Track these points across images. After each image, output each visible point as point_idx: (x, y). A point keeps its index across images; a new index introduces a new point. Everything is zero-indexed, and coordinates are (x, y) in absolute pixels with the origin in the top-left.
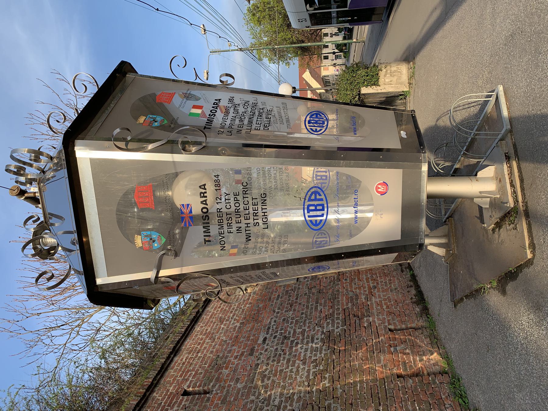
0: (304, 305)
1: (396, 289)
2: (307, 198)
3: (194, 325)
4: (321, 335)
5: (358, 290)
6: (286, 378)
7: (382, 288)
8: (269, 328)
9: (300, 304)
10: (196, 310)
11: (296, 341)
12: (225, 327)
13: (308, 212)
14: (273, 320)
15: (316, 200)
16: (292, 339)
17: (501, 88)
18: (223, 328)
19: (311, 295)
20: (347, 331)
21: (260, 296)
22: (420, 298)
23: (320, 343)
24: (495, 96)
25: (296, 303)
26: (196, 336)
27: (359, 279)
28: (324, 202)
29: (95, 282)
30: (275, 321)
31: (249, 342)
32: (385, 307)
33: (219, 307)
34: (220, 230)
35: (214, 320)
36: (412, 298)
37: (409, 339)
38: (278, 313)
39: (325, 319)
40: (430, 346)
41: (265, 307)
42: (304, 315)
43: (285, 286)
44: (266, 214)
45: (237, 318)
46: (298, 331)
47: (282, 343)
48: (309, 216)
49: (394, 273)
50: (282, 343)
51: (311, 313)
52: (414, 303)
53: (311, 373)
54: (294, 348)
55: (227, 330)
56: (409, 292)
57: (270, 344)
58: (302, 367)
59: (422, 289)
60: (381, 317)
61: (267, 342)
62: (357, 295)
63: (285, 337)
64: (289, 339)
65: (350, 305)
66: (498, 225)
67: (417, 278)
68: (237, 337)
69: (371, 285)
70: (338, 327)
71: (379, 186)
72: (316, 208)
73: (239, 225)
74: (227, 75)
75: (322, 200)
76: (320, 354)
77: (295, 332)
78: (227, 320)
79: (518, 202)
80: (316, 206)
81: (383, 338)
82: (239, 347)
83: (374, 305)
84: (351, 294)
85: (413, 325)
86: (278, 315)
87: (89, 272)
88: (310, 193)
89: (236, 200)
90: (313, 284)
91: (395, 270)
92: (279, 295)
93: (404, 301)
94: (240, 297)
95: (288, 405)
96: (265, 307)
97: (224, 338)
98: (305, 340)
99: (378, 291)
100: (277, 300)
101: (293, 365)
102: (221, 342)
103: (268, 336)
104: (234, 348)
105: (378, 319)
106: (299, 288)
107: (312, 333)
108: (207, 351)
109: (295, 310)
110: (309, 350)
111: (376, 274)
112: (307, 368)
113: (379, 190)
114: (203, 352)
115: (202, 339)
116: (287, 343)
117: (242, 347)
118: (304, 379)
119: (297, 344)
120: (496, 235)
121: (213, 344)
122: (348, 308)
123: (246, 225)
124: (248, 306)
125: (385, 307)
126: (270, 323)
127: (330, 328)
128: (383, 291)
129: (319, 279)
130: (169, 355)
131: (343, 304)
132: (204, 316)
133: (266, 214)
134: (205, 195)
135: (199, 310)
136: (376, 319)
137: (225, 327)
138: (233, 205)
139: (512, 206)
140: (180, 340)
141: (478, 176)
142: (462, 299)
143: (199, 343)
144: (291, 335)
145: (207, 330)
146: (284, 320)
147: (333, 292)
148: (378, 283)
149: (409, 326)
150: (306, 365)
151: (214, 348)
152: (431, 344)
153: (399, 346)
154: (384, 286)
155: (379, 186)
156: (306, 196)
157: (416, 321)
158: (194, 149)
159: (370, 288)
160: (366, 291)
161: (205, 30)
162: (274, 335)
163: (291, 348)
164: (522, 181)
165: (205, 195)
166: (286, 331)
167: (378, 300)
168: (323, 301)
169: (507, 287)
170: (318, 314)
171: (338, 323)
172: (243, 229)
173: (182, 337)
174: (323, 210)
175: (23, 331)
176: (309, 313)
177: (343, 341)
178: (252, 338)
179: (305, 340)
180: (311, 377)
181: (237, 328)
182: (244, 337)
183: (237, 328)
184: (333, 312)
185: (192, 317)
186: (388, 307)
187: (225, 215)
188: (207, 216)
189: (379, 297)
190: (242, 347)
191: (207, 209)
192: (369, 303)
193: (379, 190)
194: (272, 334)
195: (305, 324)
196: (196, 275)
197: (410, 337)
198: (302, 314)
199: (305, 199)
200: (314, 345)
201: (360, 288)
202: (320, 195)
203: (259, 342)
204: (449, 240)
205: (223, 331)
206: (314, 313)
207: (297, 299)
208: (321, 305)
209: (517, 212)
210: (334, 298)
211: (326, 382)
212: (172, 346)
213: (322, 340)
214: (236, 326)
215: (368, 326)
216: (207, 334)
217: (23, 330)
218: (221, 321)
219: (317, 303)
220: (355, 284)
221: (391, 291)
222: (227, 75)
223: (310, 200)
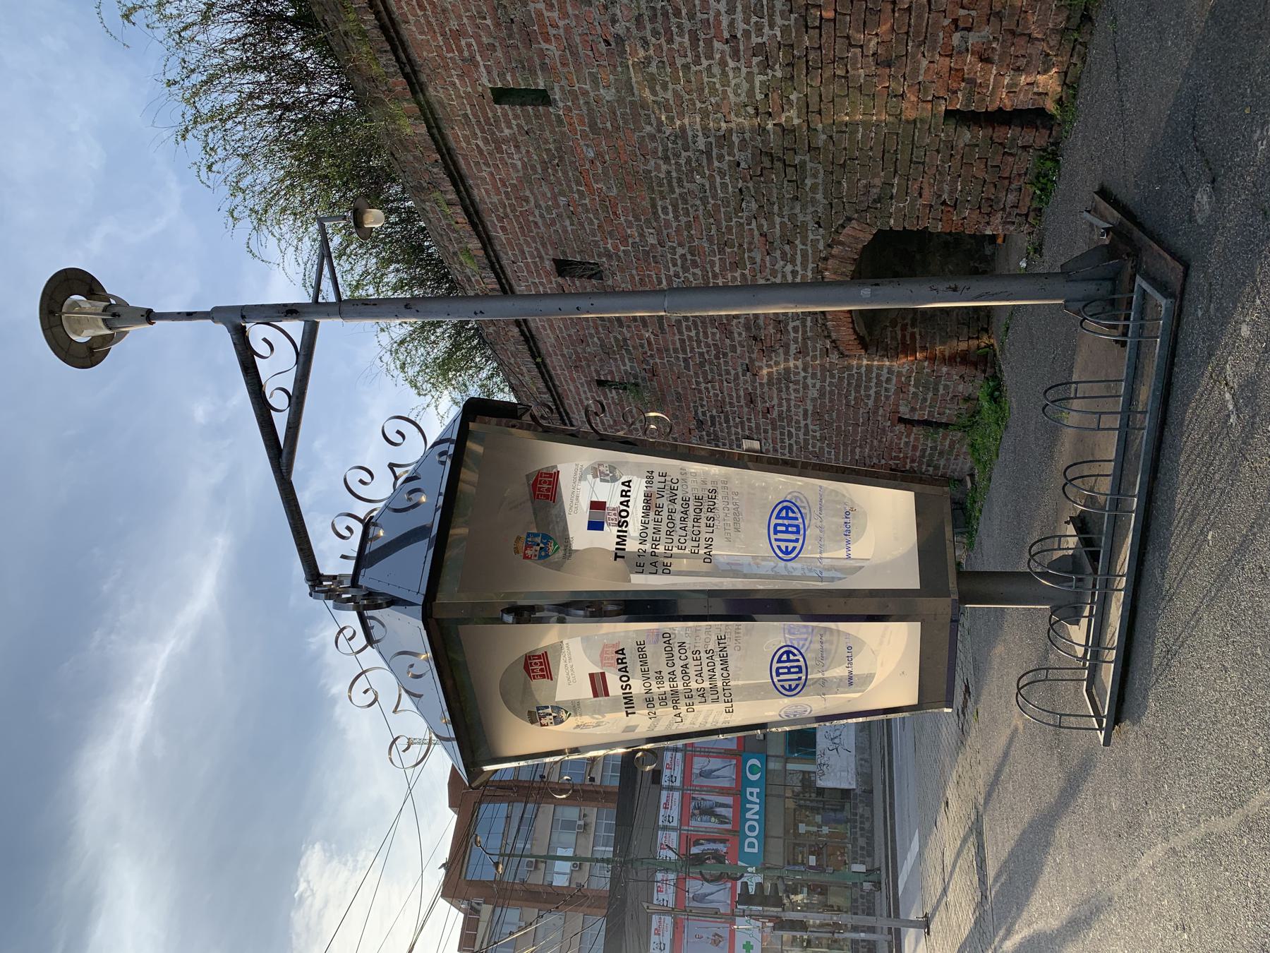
6: (703, 90)
15: (787, 518)
53: (757, 84)
58: (731, 64)
74: (343, 537)
75: (796, 519)
76: (771, 26)
80: (787, 526)
95: (725, 151)
101: (710, 57)
112: (744, 70)
118: (743, 98)
150: (742, 61)
161: (395, 740)
180: (759, 97)
211: (793, 113)
222: (343, 537)
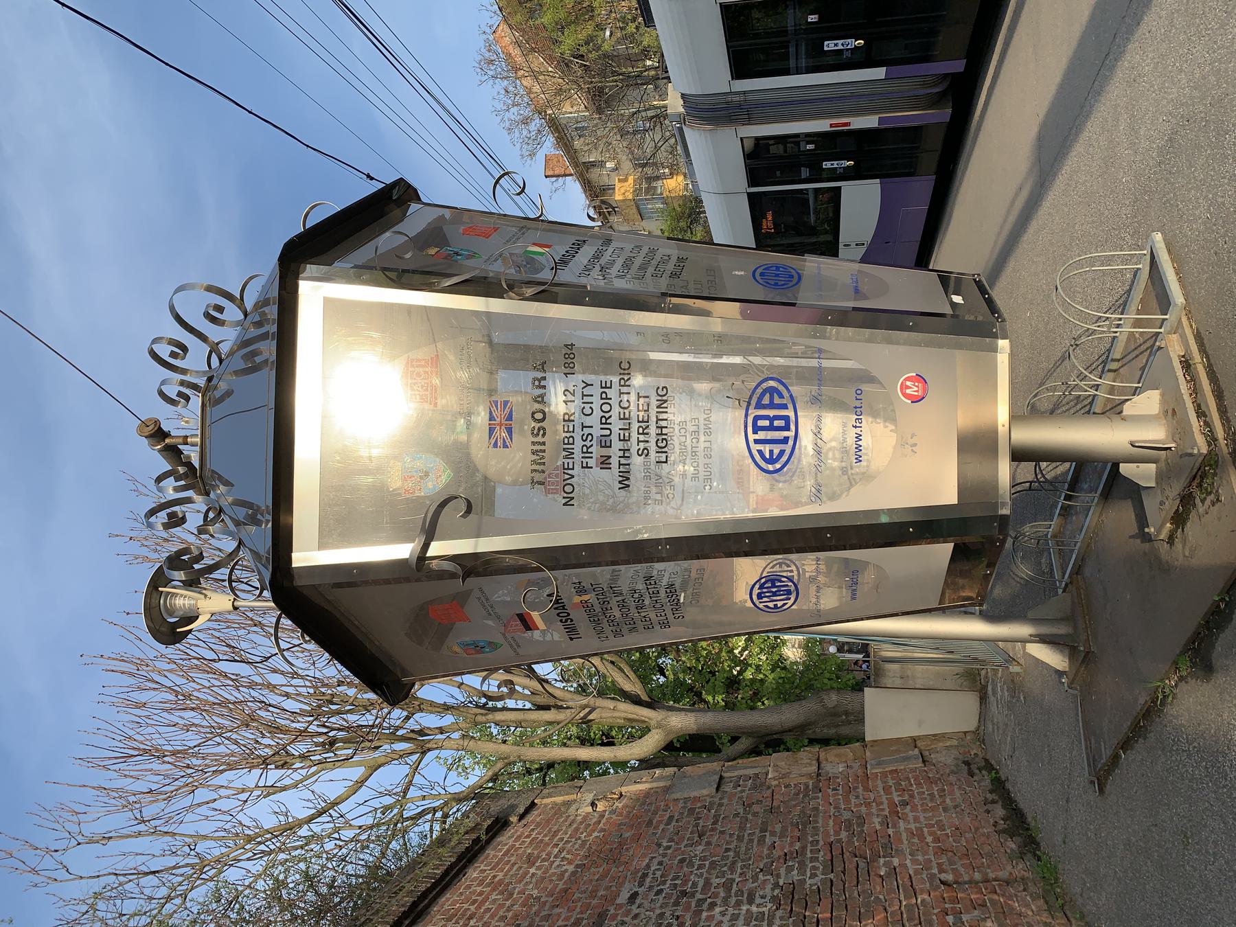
0: (731, 835)
1: (955, 807)
2: (754, 402)
3: (465, 867)
4: (773, 890)
5: (863, 809)
7: (922, 805)
8: (645, 876)
9: (722, 832)
10: (474, 836)
11: (709, 900)
12: (539, 873)
13: (755, 432)
14: (655, 861)
15: (772, 406)
16: (699, 896)
17: (1158, 237)
18: (533, 874)
19: (750, 816)
20: (838, 885)
21: (627, 817)
22: (1017, 823)
23: (769, 905)
24: (1148, 257)
25: (712, 830)
26: (469, 887)
27: (866, 789)
28: (791, 414)
29: (289, 560)
30: (660, 863)
31: (594, 902)
32: (929, 839)
33: (528, 836)
34: (566, 461)
35: (513, 859)
36: (995, 824)
37: (991, 900)
38: (669, 848)
39: (782, 861)
40: (1045, 914)
41: (637, 838)
42: (731, 854)
43: (686, 800)
44: (665, 431)
45: (569, 856)
46: (715, 881)
47: (676, 904)
48: (756, 442)
49: (952, 778)
50: (676, 904)
51: (747, 849)
52: (1004, 831)
54: (705, 914)
55: (543, 878)
56: (988, 812)
57: (646, 904)
59: (1021, 805)
60: (920, 858)
61: (638, 901)
62: (860, 817)
63: (684, 893)
64: (693, 895)
65: (844, 835)
66: (1179, 519)
67: (1008, 786)
68: (566, 891)
69: (897, 799)
70: (813, 876)
71: (908, 383)
72: (771, 423)
73: (605, 452)
75: (785, 407)
77: (707, 883)
78: (544, 860)
79: (1215, 440)
80: (772, 419)
81: (926, 896)
82: (571, 910)
83: (904, 836)
84: (847, 815)
85: (1002, 874)
86: (669, 851)
87: (282, 541)
88: (759, 391)
89: (605, 398)
90: (756, 796)
91: (953, 772)
92: (671, 818)
93: (977, 829)
94: (579, 818)
96: (637, 838)
97: (536, 891)
98: (733, 900)
99: (914, 809)
100: (668, 824)
102: (527, 899)
103: (641, 890)
104: (557, 910)
105: (914, 862)
106: (720, 805)
107: (750, 885)
108: (492, 917)
109: (709, 843)
110: (742, 918)
111: (908, 779)
113: (908, 391)
114: (482, 918)
115: (480, 894)
116: (689, 904)
117: (578, 910)
119: (712, 906)
120: (1178, 545)
121: (508, 903)
122: (839, 841)
123: (621, 453)
124: (596, 834)
125: (929, 839)
126: (648, 866)
127: (795, 876)
128: (924, 811)
129: (769, 788)
130: (400, 918)
131: (827, 834)
132: (490, 852)
133: (665, 431)
134: (543, 383)
135: (478, 838)
136: (908, 862)
137: (539, 873)
138: (596, 406)
139: (1204, 450)
140: (428, 891)
141: (1124, 413)
142: (1115, 758)
143: (474, 902)
144: (699, 889)
145: (495, 877)
146: (682, 861)
147: (802, 811)
148: (912, 796)
149: (991, 875)
151: (508, 911)
152: (1049, 910)
153: (968, 912)
154: (927, 801)
155: (908, 383)
156: (751, 398)
157: (1009, 868)
158: (529, 291)
159: (892, 804)
160: (883, 810)
162: (656, 889)
163: (698, 913)
164: (1219, 395)
165: (543, 383)
166: (685, 882)
167: (912, 826)
168: (778, 828)
169: (1214, 655)
170: (766, 852)
171: (814, 868)
172: (614, 461)
173: (434, 886)
174: (787, 428)
175: (62, 874)
176: (743, 849)
177: (826, 903)
178: (602, 893)
179: (733, 900)
181: (567, 875)
182: (582, 893)
183: (567, 875)
184: (804, 848)
185: (462, 848)
186: (937, 840)
187: (578, 429)
188: (544, 429)
189: (916, 820)
190: (578, 910)
191: (544, 413)
192: (890, 831)
193: (908, 391)
194: (651, 888)
195: (732, 868)
196: (509, 559)
197: (996, 897)
198: (727, 850)
199: (749, 404)
200: (754, 909)
201: (868, 805)
202: (781, 396)
203: (619, 901)
204: (1075, 628)
205: (534, 880)
206: (755, 849)
207: (714, 823)
208: (773, 834)
209: (1217, 462)
210: (807, 821)
212: (409, 900)
213: (774, 899)
214: (566, 871)
215: (888, 874)
216: (494, 885)
217: (64, 871)
218: (531, 861)
219: (763, 830)
220: (857, 797)
221: (945, 810)
223: (759, 406)
